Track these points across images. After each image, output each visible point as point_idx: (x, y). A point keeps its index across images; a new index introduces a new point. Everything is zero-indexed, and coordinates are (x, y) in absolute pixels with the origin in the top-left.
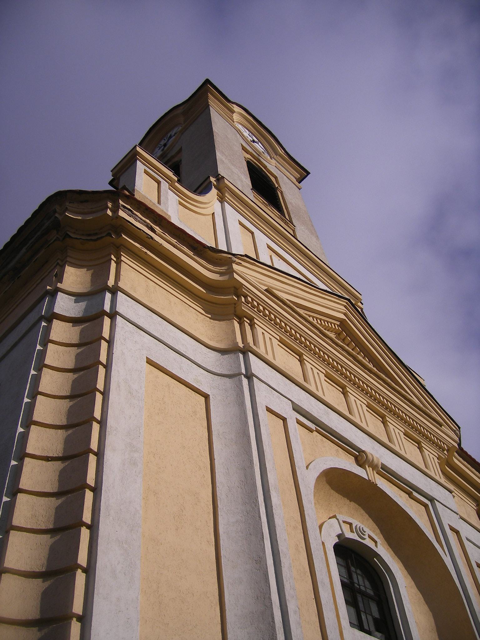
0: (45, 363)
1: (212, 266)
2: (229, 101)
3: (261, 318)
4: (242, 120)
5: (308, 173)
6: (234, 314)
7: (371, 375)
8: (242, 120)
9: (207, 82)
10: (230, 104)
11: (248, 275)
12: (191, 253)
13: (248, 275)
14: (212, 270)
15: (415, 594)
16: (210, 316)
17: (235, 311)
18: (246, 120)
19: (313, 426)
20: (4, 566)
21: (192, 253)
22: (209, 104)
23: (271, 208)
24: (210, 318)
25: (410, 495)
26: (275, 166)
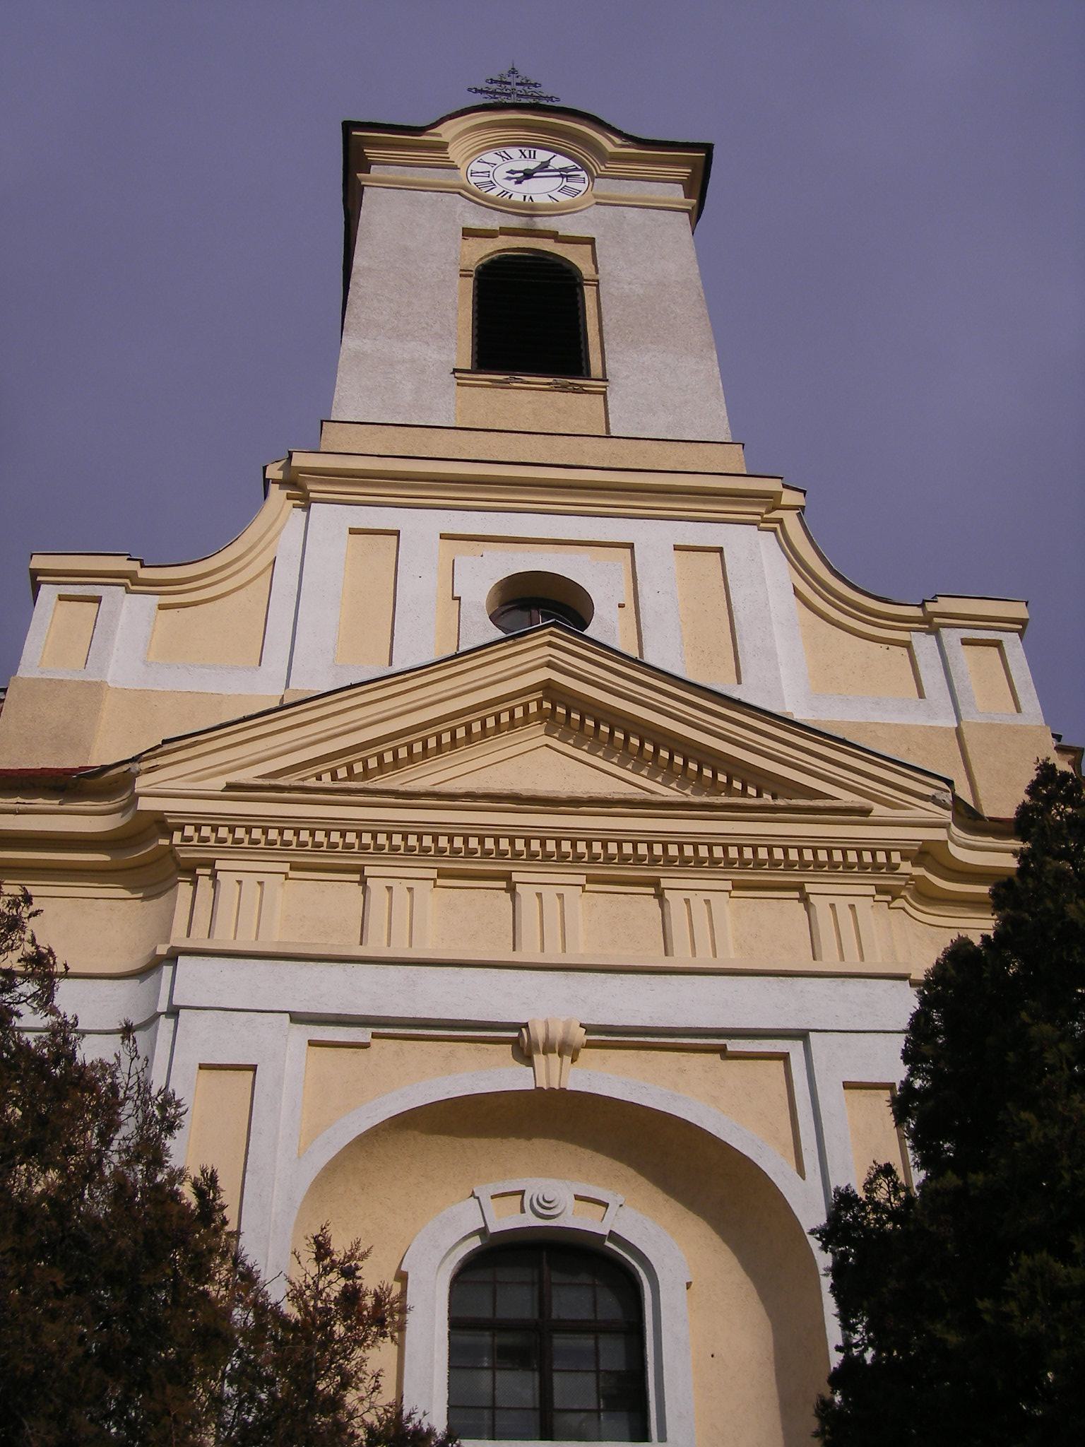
0: (174, 1003)
1: (107, 803)
2: (421, 130)
3: (229, 852)
4: (490, 135)
5: (708, 148)
6: (181, 870)
7: (580, 809)
8: (490, 135)
9: (348, 126)
10: (428, 135)
11: (159, 782)
12: (53, 804)
13: (159, 782)
14: (110, 810)
15: (738, 1285)
16: (141, 895)
17: (178, 865)
18: (501, 127)
19: (362, 1035)
20: (554, 1316)
21: (57, 802)
22: (363, 183)
23: (521, 383)
24: (142, 899)
25: (722, 1051)
26: (597, 203)
